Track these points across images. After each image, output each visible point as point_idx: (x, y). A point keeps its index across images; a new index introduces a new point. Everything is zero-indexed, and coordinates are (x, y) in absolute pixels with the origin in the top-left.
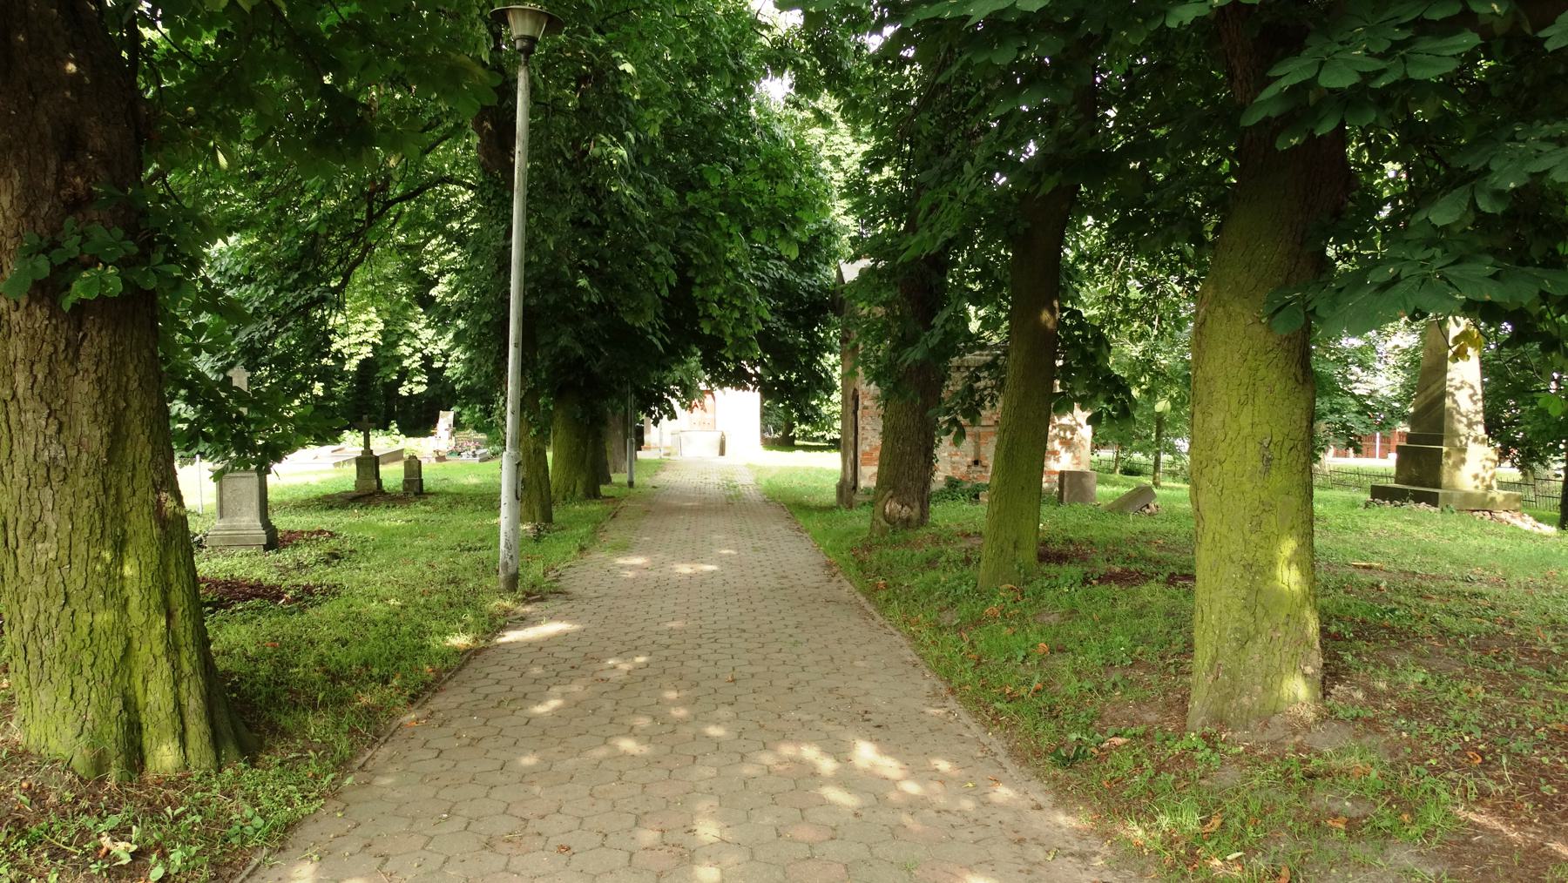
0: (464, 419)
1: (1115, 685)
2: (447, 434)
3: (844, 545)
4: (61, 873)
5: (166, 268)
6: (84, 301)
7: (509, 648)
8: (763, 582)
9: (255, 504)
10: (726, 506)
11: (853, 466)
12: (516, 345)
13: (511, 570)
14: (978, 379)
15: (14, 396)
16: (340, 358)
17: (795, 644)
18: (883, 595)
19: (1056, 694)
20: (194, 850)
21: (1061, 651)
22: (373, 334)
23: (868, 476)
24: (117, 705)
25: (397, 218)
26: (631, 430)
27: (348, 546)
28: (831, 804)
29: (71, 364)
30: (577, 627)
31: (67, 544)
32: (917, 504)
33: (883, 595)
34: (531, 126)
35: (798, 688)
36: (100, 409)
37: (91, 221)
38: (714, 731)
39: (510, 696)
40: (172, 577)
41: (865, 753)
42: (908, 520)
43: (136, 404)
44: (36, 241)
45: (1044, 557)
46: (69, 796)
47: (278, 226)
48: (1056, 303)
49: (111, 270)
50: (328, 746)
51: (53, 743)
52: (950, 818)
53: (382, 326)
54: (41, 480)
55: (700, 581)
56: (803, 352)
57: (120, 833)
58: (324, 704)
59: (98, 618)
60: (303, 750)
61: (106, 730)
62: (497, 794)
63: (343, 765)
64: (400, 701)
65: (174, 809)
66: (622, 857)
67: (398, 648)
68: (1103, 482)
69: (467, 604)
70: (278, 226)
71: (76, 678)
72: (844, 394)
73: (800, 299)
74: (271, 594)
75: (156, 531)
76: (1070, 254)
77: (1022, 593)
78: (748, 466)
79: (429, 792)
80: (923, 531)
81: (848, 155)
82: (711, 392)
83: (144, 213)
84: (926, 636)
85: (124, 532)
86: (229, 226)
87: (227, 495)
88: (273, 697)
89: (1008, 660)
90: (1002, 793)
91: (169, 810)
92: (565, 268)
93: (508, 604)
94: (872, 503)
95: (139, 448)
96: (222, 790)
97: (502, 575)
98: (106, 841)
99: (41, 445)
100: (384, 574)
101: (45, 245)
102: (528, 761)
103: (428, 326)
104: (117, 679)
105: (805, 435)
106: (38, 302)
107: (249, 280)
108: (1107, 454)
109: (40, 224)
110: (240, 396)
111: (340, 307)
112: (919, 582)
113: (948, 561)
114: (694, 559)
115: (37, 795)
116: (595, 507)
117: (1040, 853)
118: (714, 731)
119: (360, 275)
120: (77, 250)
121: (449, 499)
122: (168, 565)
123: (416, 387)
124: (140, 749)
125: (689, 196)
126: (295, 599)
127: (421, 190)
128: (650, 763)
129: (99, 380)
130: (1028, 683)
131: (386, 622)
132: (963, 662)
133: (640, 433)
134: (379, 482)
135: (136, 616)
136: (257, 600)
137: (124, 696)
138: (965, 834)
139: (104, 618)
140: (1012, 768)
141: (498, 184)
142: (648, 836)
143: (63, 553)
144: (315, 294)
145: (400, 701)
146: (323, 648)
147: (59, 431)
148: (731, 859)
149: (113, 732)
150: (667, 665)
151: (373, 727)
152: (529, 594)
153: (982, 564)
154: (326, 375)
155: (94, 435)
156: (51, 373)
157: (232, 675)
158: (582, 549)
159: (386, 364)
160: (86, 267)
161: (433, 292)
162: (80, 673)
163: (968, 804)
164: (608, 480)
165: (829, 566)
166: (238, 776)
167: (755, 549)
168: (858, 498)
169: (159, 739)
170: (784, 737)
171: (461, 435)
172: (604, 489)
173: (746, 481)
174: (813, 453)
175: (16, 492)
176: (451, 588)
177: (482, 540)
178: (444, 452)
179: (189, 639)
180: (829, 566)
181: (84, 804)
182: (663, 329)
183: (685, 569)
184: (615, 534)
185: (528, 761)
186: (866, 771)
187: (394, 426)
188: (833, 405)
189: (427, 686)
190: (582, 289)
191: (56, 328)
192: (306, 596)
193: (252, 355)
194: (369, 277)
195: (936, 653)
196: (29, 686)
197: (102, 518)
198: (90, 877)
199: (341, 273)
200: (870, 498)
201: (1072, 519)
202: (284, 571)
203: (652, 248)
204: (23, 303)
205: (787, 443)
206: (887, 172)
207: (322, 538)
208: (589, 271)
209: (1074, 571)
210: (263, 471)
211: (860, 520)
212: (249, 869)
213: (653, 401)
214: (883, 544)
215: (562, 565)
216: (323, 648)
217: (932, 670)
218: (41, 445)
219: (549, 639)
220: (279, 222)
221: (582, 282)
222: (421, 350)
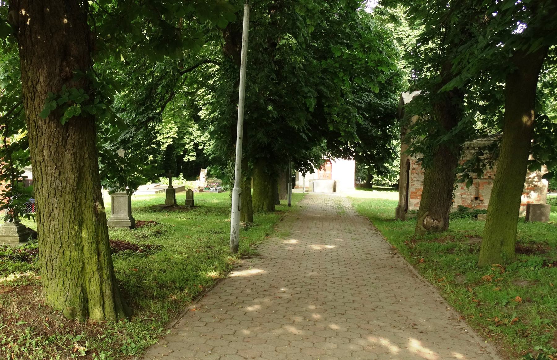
0: (212, 172)
2: (204, 179)
3: (401, 239)
4: (61, 356)
5: (100, 105)
8: (357, 256)
9: (126, 208)
10: (337, 217)
11: (405, 199)
12: (240, 138)
13: (235, 244)
14: (482, 154)
15: (44, 160)
16: (158, 144)
17: (376, 287)
18: (423, 266)
20: (109, 353)
21: (530, 301)
22: (173, 133)
23: (414, 204)
24: (79, 290)
26: (290, 179)
27: (164, 229)
29: (64, 147)
31: (62, 222)
32: (442, 219)
33: (423, 266)
35: (378, 309)
36: (74, 166)
37: (72, 86)
38: (334, 327)
39: (237, 301)
40: (100, 238)
42: (437, 228)
43: (87, 164)
44: (52, 95)
45: (519, 250)
46: (62, 326)
47: (137, 85)
48: (533, 112)
50: (159, 317)
51: (56, 303)
53: (177, 129)
54: (53, 195)
55: (323, 254)
56: (380, 139)
59: (73, 253)
60: (150, 317)
61: (75, 300)
62: (232, 345)
63: (165, 325)
64: (188, 299)
65: (101, 336)
67: (187, 276)
69: (216, 257)
70: (137, 85)
72: (402, 160)
73: (380, 112)
74: (134, 248)
75: (94, 218)
77: (505, 269)
78: (348, 198)
79: (202, 340)
80: (445, 234)
81: (407, 37)
84: (448, 288)
85: (82, 218)
86: (119, 86)
87: (116, 204)
88: (136, 292)
89: (497, 304)
91: (99, 336)
92: (262, 101)
93: (234, 259)
94: (415, 218)
95: (88, 183)
96: (119, 330)
97: (231, 246)
98: (76, 345)
99: (53, 181)
100: (180, 243)
101: (55, 97)
103: (198, 130)
104: (80, 279)
105: (378, 182)
106: (52, 121)
107: (124, 110)
109: (54, 88)
110: (121, 160)
111: (160, 121)
112: (445, 259)
113: (460, 250)
114: (323, 242)
115: (51, 324)
116: (272, 216)
118: (334, 327)
119: (169, 106)
120: (67, 99)
121: (205, 209)
122: (98, 233)
123: (191, 157)
124: (88, 309)
125: (323, 62)
126: (143, 251)
128: (305, 339)
129: (74, 154)
130: (509, 317)
131: (181, 263)
132: (470, 303)
133: (294, 180)
134: (175, 200)
135: (87, 254)
136: (128, 250)
137: (82, 286)
139: (75, 254)
141: (231, 62)
143: (60, 226)
144: (151, 116)
145: (188, 299)
146: (155, 273)
147: (60, 175)
149: (78, 300)
150: (310, 293)
151: (177, 310)
152: (243, 255)
153: (481, 252)
154: (155, 152)
155: (72, 177)
156: (56, 151)
157: (120, 282)
158: (267, 235)
159: (178, 147)
160: (70, 106)
161: (199, 114)
162: (66, 276)
164: (278, 203)
165: (392, 249)
166: (124, 325)
167: (353, 239)
168: (408, 215)
169: (95, 306)
171: (210, 180)
173: (346, 204)
174: (382, 192)
175: (44, 200)
176: (208, 250)
177: (221, 229)
178: (202, 187)
179: (106, 265)
180: (392, 249)
181: (68, 329)
182: (308, 129)
183: (316, 247)
184: (282, 228)
185: (246, 332)
186: (415, 354)
187: (181, 176)
188: (396, 165)
189: (200, 294)
190: (270, 111)
191: (59, 132)
192: (148, 250)
193: (124, 143)
194: (172, 107)
195: (453, 297)
196: (48, 279)
197: (75, 212)
198: (71, 359)
199: (161, 106)
200: (415, 215)
201: (535, 230)
202: (138, 238)
203: (306, 89)
204: (47, 122)
205: (368, 186)
206: (431, 45)
208: (273, 102)
209: (538, 259)
210: (130, 193)
211: (409, 227)
213: (304, 163)
214: (422, 239)
215: (258, 242)
216: (155, 273)
217: (451, 306)
218: (53, 181)
219: (253, 277)
220: (137, 84)
221: (270, 108)
222: (193, 141)
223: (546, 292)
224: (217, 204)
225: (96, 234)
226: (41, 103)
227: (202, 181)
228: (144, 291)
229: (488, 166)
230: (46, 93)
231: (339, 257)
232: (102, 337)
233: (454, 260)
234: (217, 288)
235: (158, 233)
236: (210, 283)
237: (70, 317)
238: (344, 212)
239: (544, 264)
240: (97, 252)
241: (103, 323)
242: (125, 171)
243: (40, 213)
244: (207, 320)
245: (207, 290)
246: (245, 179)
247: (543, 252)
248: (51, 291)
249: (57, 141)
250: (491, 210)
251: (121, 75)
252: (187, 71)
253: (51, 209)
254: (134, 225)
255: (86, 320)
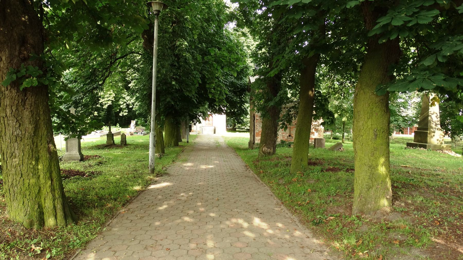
0: (139, 123)
1: (331, 201)
2: (134, 127)
4: (20, 256)
5: (51, 78)
6: (26, 87)
7: (152, 190)
8: (227, 171)
9: (77, 148)
10: (216, 148)
12: (154, 101)
13: (152, 167)
14: (290, 111)
15: (6, 116)
16: (102, 105)
18: (262, 175)
19: (313, 204)
20: (59, 249)
21: (315, 191)
23: (258, 140)
24: (37, 207)
25: (119, 64)
27: (104, 160)
28: (247, 236)
29: (23, 106)
30: (172, 184)
31: (22, 159)
32: (272, 148)
33: (262, 175)
34: (158, 36)
35: (237, 202)
36: (31, 120)
37: (29, 65)
38: (212, 215)
39: (153, 204)
40: (53, 169)
41: (257, 221)
42: (270, 153)
43: (42, 118)
45: (310, 164)
46: (22, 233)
48: (313, 89)
49: (35, 79)
51: (17, 218)
52: (282, 240)
53: (114, 95)
56: (239, 103)
57: (37, 244)
58: (97, 207)
59: (31, 181)
60: (91, 220)
62: (148, 233)
63: (103, 225)
64: (120, 206)
66: (185, 252)
68: (327, 142)
69: (139, 177)
71: (24, 199)
73: (238, 88)
74: (82, 174)
75: (48, 156)
76: (317, 74)
77: (303, 174)
78: (222, 137)
79: (128, 232)
80: (274, 156)
81: (252, 45)
82: (210, 115)
83: (44, 62)
84: (275, 187)
85: (39, 156)
88: (82, 205)
89: (299, 194)
90: (297, 233)
91: (52, 238)
93: (151, 177)
95: (43, 131)
96: (67, 232)
97: (150, 169)
98: (33, 247)
99: (14, 130)
100: (115, 168)
101: (15, 71)
102: (157, 223)
103: (128, 95)
104: (37, 199)
106: (13, 88)
107: (75, 82)
108: (329, 133)
109: (14, 65)
110: (73, 116)
111: (102, 90)
113: (281, 165)
114: (207, 164)
115: (13, 233)
116: (177, 149)
117: (308, 251)
118: (212, 215)
122: (51, 165)
123: (124, 113)
124: (43, 220)
126: (89, 176)
127: (127, 55)
129: (31, 111)
130: (305, 201)
131: (116, 182)
133: (190, 127)
134: (114, 141)
135: (42, 180)
136: (78, 176)
137: (38, 204)
138: (286, 245)
139: (33, 181)
140: (300, 226)
141: (149, 54)
142: (193, 246)
143: (21, 162)
144: (95, 86)
145: (120, 206)
146: (97, 190)
147: (20, 126)
148: (217, 252)
149: (35, 215)
150: (199, 195)
151: (112, 213)
152: (158, 174)
154: (98, 110)
155: (30, 127)
156: (17, 109)
157: (70, 198)
158: (173, 161)
159: (116, 107)
160: (27, 78)
161: (129, 85)
162: (26, 197)
163: (287, 236)
164: (181, 141)
165: (246, 166)
166: (72, 227)
167: (224, 161)
169: (49, 217)
170: (233, 216)
172: (180, 143)
173: (221, 141)
174: (241, 133)
175: (7, 144)
177: (144, 158)
178: (133, 132)
179: (58, 187)
180: (246, 166)
181: (27, 236)
182: (197, 97)
183: (203, 167)
184: (183, 157)
185: (157, 223)
186: (257, 227)
187: (118, 125)
189: (128, 201)
190: (174, 85)
193: (76, 104)
195: (278, 192)
196: (11, 201)
197: (32, 151)
198: (28, 257)
201: (318, 153)
202: (85, 167)
204: (9, 88)
205: (234, 130)
206: (263, 50)
207: (97, 158)
208: (176, 80)
209: (318, 168)
210: (80, 138)
212: (75, 255)
214: (262, 160)
216: (97, 190)
217: (277, 197)
218: (14, 130)
220: (84, 65)
221: (174, 83)
222: (126, 103)
223: (322, 186)
224: (142, 142)
225: (50, 166)
226: (4, 75)
227: (132, 127)
228: (88, 203)
229: (293, 118)
230: (7, 68)
231: (216, 172)
232: (54, 238)
233: (278, 171)
234: (139, 197)
235: (100, 163)
236: (135, 194)
237: (29, 227)
238: (220, 145)
239: (322, 171)
240: (50, 179)
241: (55, 228)
242: (75, 124)
243: (3, 154)
244: (132, 218)
245: (133, 198)
246: (159, 126)
247: (321, 164)
248: (13, 209)
249: (17, 102)
250: (295, 142)
251: (73, 58)
252: (120, 58)
253: (13, 150)
254: (83, 159)
255: (42, 228)
